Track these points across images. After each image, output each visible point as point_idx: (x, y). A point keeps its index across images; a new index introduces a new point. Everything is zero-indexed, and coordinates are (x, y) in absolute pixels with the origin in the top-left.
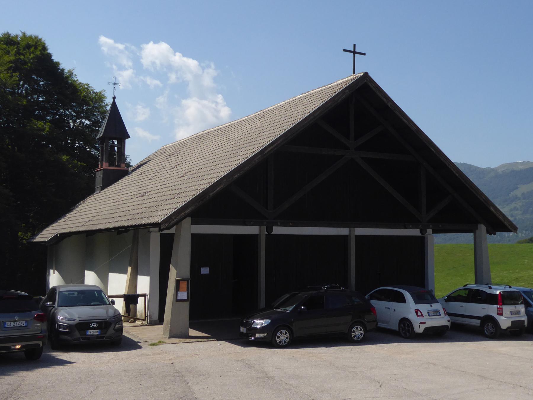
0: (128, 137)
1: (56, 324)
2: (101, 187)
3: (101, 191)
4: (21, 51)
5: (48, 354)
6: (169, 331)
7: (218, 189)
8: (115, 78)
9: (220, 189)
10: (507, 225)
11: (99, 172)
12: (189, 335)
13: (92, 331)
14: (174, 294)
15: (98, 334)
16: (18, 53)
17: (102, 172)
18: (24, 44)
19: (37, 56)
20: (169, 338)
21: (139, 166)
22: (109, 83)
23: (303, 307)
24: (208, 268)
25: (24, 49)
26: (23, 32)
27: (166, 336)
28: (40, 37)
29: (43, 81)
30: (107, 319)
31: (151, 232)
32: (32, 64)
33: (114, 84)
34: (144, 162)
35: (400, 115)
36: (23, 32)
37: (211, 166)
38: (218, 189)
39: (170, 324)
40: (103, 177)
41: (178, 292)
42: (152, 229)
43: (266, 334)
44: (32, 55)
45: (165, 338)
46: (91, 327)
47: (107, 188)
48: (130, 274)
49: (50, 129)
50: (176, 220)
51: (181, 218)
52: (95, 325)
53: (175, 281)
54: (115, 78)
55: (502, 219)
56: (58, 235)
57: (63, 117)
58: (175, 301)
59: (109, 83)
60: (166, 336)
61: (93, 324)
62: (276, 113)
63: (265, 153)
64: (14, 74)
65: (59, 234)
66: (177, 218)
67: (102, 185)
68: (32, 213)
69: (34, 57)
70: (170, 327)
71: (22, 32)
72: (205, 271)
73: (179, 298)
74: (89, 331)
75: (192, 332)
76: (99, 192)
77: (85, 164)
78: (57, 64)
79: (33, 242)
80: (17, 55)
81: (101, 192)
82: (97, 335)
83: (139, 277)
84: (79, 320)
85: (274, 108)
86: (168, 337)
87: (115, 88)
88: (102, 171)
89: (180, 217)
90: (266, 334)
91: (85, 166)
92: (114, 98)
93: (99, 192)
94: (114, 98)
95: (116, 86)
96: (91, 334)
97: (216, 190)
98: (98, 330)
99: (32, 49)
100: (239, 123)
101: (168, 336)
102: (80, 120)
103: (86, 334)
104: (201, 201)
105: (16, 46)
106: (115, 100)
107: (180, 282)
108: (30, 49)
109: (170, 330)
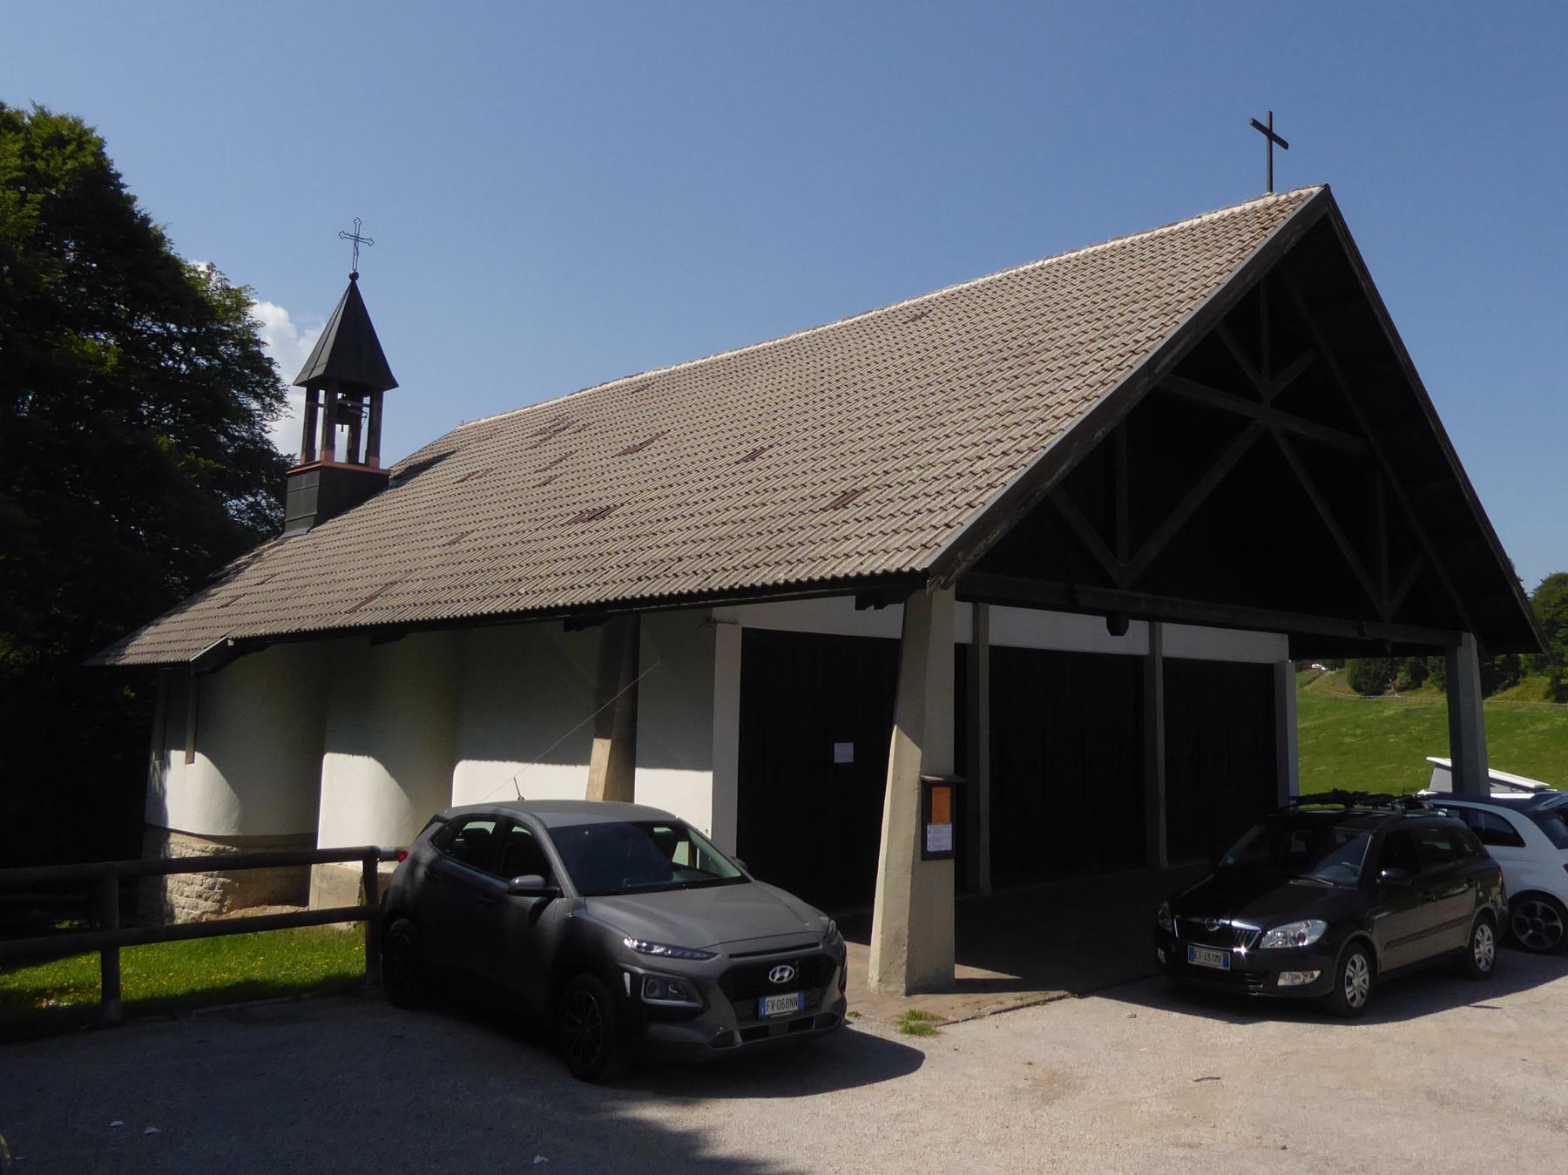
0: (393, 384)
1: (623, 978)
3: (312, 528)
4: (37, 151)
5: (625, 1121)
6: (904, 967)
7: (1060, 471)
8: (357, 222)
9: (1065, 470)
10: (1536, 634)
11: (304, 476)
12: (956, 977)
13: (776, 999)
14: (915, 835)
15: (796, 1008)
16: (28, 152)
17: (317, 473)
18: (46, 132)
19: (84, 166)
20: (909, 993)
21: (413, 470)
23: (1384, 873)
24: (852, 744)
25: (45, 147)
26: (38, 104)
27: (891, 988)
28: (87, 125)
30: (818, 945)
31: (716, 622)
32: (67, 185)
33: (357, 239)
34: (421, 459)
35: (1382, 322)
36: (38, 104)
38: (1060, 471)
39: (907, 943)
41: (928, 827)
42: (717, 612)
43: (1316, 974)
44: (70, 164)
45: (893, 993)
46: (775, 981)
47: (330, 520)
48: (605, 763)
49: (120, 361)
50: (965, 564)
51: (979, 557)
52: (786, 974)
53: (917, 786)
55: (1529, 620)
56: (230, 643)
58: (919, 858)
59: (342, 235)
60: (891, 988)
61: (778, 968)
63: (1157, 372)
64: (29, 196)
65: (233, 639)
66: (968, 558)
67: (315, 513)
68: (61, 589)
69: (74, 169)
70: (909, 950)
71: (34, 105)
72: (844, 753)
73: (931, 847)
74: (767, 999)
75: (963, 972)
76: (308, 532)
78: (131, 200)
79: (114, 667)
80: (27, 158)
82: (795, 1013)
83: (638, 771)
84: (731, 956)
85: (684, 371)
86: (903, 989)
88: (317, 473)
89: (975, 556)
90: (1316, 974)
92: (354, 277)
94: (354, 277)
95: (360, 245)
96: (776, 1011)
97: (1057, 474)
98: (795, 995)
99: (71, 148)
100: (524, 416)
101: (904, 985)
103: (756, 1014)
104: (1021, 506)
105: (22, 135)
106: (357, 281)
107: (934, 789)
108: (65, 148)
109: (910, 964)
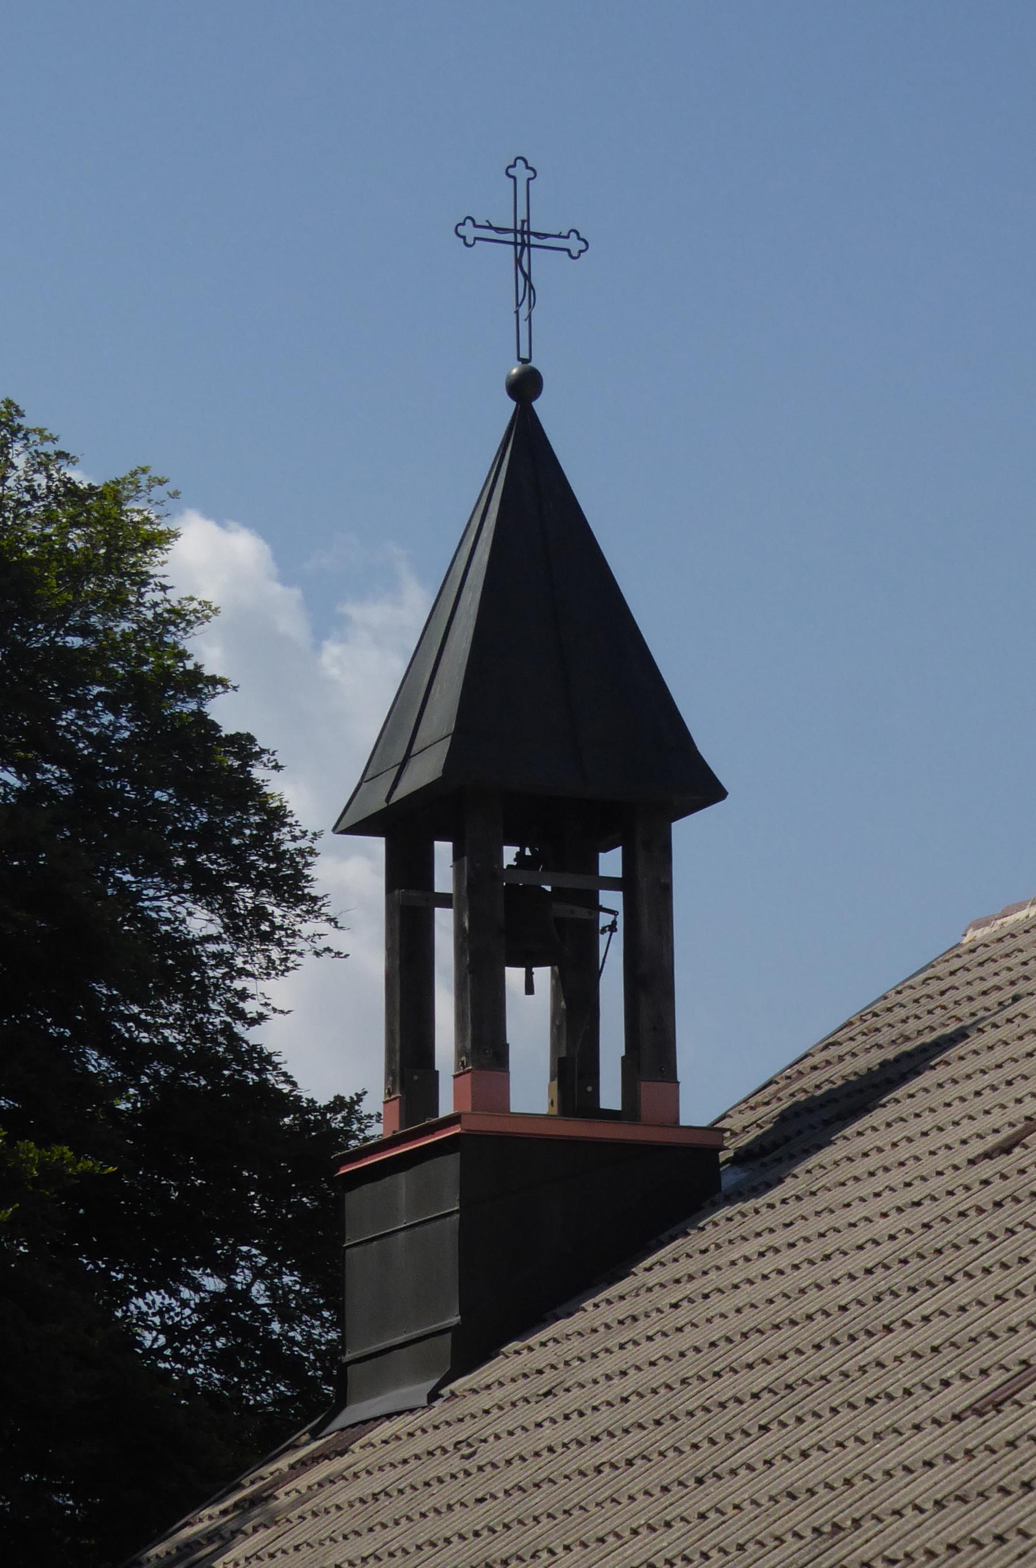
2: (398, 1100)
11: (402, 1179)
17: (451, 1165)
22: (467, 230)
29: (25, 1247)
37: (589, 1537)
40: (462, 1223)
54: (521, 172)
57: (132, 1282)
59: (467, 230)
62: (930, 1012)
67: (455, 1319)
76: (433, 1396)
77: (88, 1164)
81: (458, 1385)
87: (527, 277)
88: (451, 1165)
91: (86, 1175)
93: (433, 1396)
102: (24, 640)
